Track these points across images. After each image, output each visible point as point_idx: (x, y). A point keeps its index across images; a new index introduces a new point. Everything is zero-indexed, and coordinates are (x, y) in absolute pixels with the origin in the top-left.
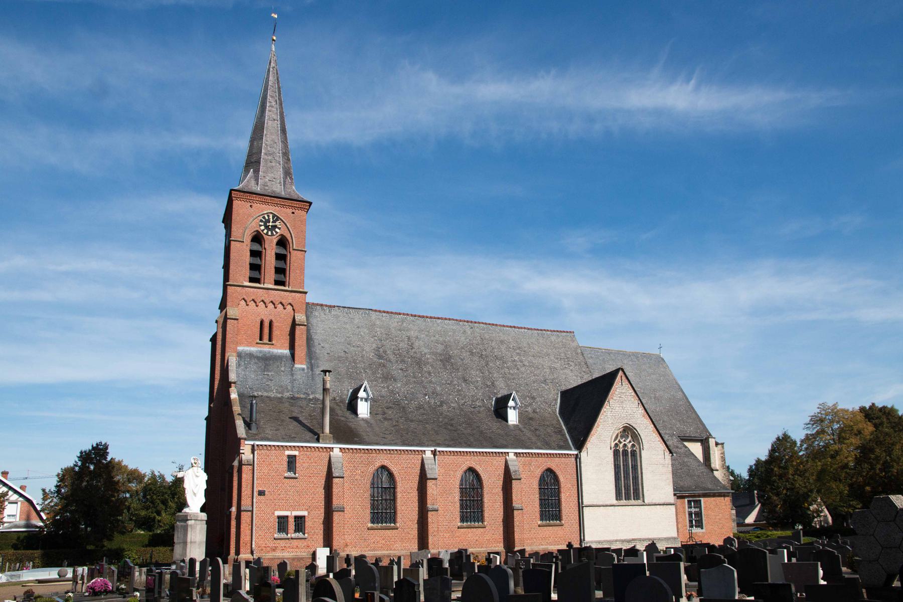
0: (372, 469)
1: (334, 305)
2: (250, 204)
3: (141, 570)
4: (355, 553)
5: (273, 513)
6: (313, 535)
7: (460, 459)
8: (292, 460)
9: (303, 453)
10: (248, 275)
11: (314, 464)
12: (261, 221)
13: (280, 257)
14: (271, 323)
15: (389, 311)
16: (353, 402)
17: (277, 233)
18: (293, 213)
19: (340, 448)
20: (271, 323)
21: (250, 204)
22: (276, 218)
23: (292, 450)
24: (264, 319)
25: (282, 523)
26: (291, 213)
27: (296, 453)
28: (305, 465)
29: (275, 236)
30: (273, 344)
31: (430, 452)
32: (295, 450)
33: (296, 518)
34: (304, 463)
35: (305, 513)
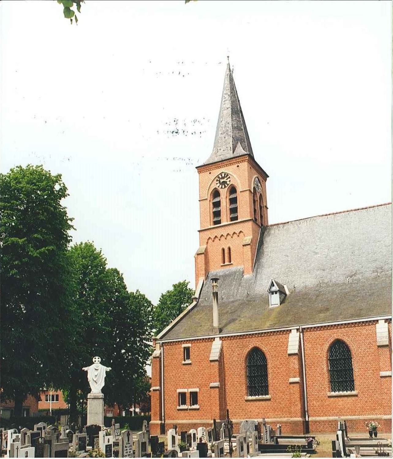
0: (246, 351)
1: (288, 221)
2: (209, 172)
3: (200, 442)
4: (235, 420)
5: (176, 391)
6: (203, 406)
7: (327, 333)
8: (187, 350)
9: (194, 344)
10: (212, 220)
11: (202, 352)
12: (217, 180)
13: (217, 204)
14: (229, 249)
15: (386, 203)
16: (283, 297)
17: (228, 185)
18: (238, 166)
19: (220, 337)
20: (229, 249)
21: (209, 172)
22: (226, 175)
23: (186, 343)
24: (224, 247)
25: (183, 396)
26: (236, 167)
27: (189, 345)
28: (196, 353)
29: (228, 187)
30: (232, 264)
31: (296, 330)
32: (189, 343)
33: (191, 393)
34: (195, 352)
35: (197, 390)
